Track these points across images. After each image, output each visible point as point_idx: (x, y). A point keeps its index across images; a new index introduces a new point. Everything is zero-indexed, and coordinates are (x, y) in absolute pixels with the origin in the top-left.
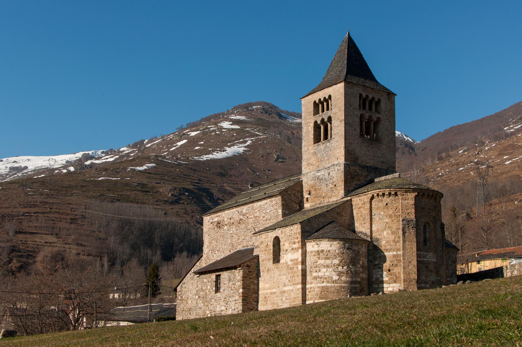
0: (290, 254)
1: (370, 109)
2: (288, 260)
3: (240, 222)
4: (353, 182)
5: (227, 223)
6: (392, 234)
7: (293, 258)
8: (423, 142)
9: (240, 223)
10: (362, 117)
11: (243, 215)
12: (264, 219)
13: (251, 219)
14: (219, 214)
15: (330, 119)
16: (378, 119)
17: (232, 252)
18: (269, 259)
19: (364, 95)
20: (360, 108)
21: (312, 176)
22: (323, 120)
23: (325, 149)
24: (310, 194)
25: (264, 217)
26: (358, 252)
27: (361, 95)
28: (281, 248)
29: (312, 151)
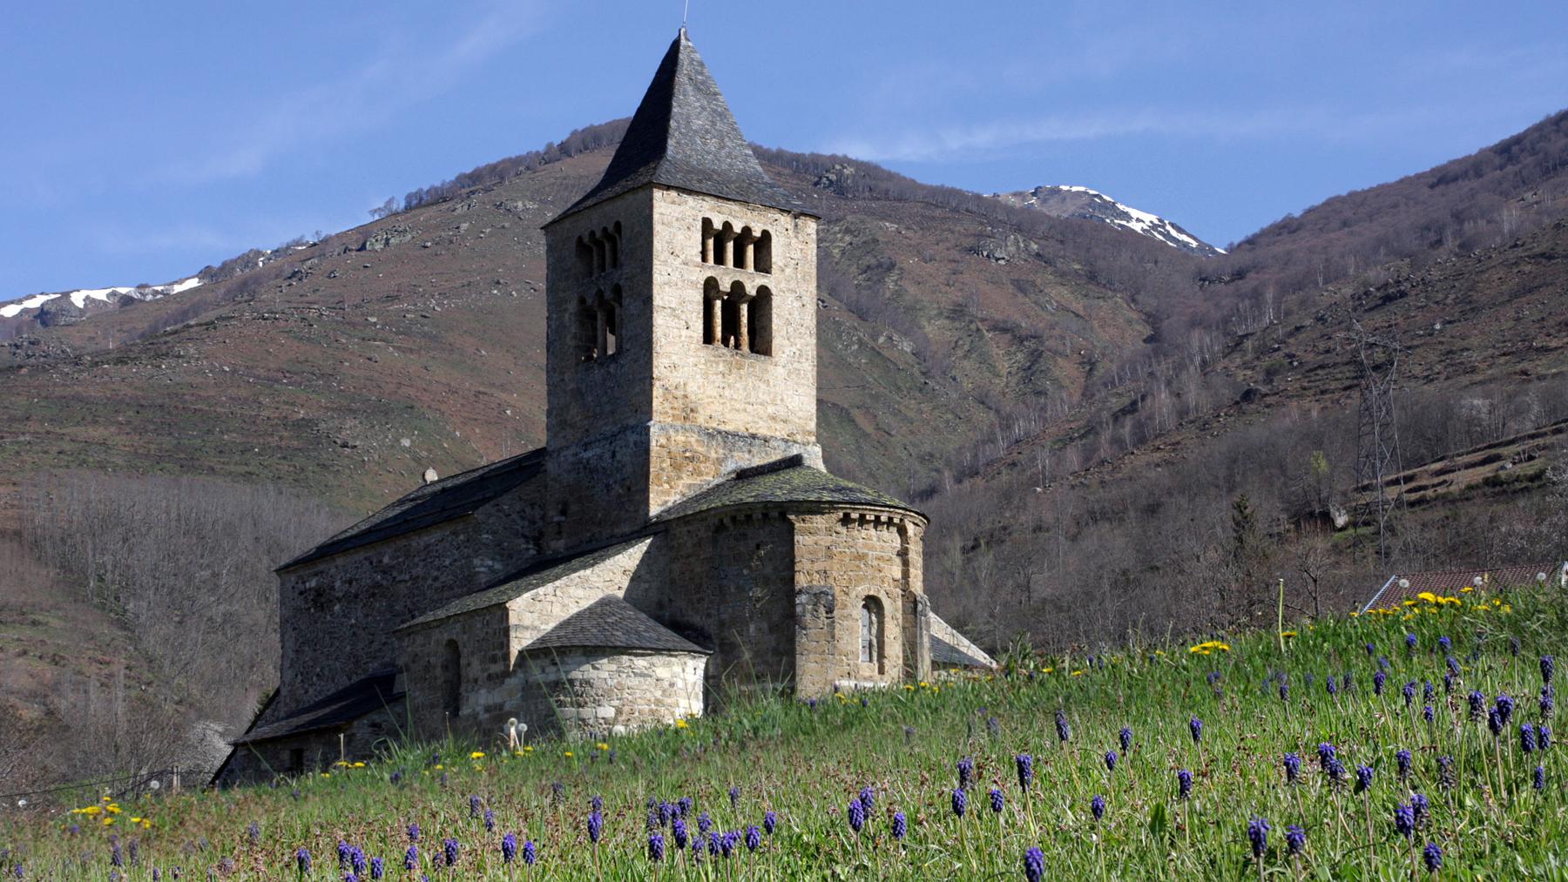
0: (483, 691)
1: (739, 262)
2: (479, 709)
3: (375, 591)
4: (679, 478)
5: (340, 595)
6: (771, 630)
7: (491, 702)
8: (1231, 249)
9: (373, 595)
10: (710, 286)
11: (384, 572)
12: (437, 584)
13: (402, 586)
14: (321, 567)
15: (617, 290)
16: (764, 292)
17: (355, 679)
18: (432, 706)
19: (718, 225)
20: (704, 259)
21: (571, 459)
22: (600, 294)
23: (604, 380)
24: (563, 513)
25: (436, 579)
26: (672, 685)
27: (707, 223)
28: (463, 673)
29: (572, 386)
